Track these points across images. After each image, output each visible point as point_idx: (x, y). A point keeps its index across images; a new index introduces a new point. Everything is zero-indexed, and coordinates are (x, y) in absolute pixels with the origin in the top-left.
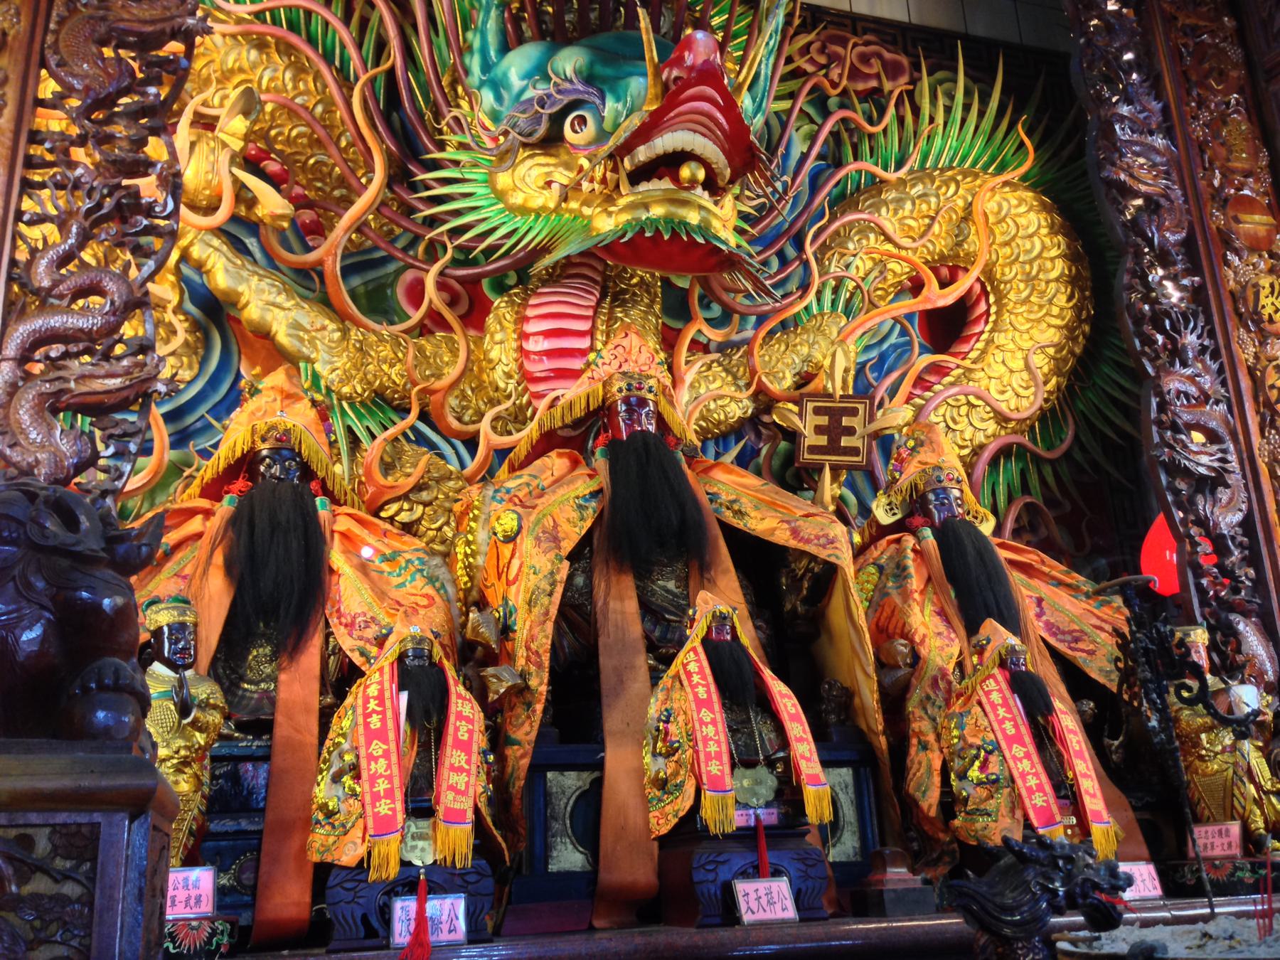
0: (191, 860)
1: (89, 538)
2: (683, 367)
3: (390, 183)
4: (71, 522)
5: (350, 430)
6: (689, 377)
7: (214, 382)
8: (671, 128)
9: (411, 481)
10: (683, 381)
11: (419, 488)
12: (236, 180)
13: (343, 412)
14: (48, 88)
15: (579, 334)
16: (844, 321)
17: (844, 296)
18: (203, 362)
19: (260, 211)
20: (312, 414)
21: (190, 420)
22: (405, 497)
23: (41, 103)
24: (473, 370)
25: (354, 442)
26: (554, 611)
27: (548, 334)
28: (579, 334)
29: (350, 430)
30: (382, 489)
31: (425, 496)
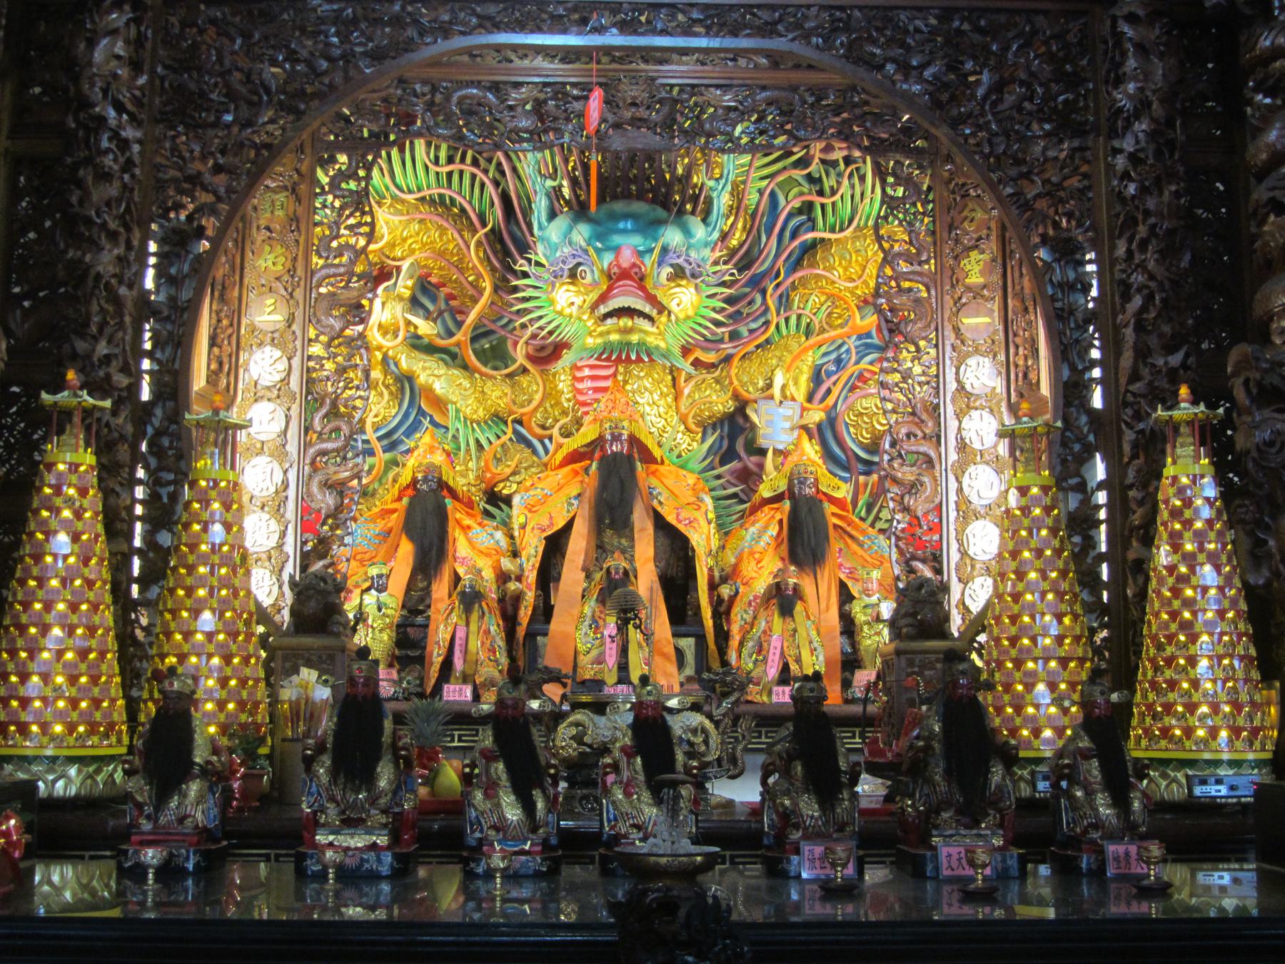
0: (258, 623)
1: (330, 587)
2: (682, 384)
3: (496, 289)
4: (325, 582)
5: (477, 441)
6: (686, 391)
7: (406, 415)
8: (614, 296)
9: (508, 471)
10: (682, 393)
11: (514, 473)
12: (406, 319)
13: (473, 429)
14: (312, 333)
15: (606, 378)
16: (803, 339)
17: (804, 324)
18: (400, 405)
19: (420, 332)
20: (444, 456)
21: (395, 437)
22: (507, 479)
23: (310, 340)
24: (550, 394)
25: (480, 446)
26: (537, 565)
27: (593, 378)
28: (606, 378)
29: (477, 441)
30: (494, 475)
31: (517, 478)
